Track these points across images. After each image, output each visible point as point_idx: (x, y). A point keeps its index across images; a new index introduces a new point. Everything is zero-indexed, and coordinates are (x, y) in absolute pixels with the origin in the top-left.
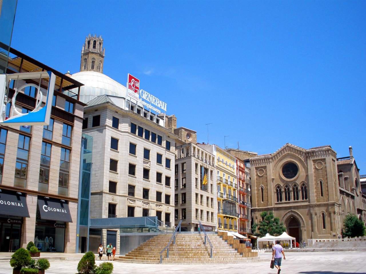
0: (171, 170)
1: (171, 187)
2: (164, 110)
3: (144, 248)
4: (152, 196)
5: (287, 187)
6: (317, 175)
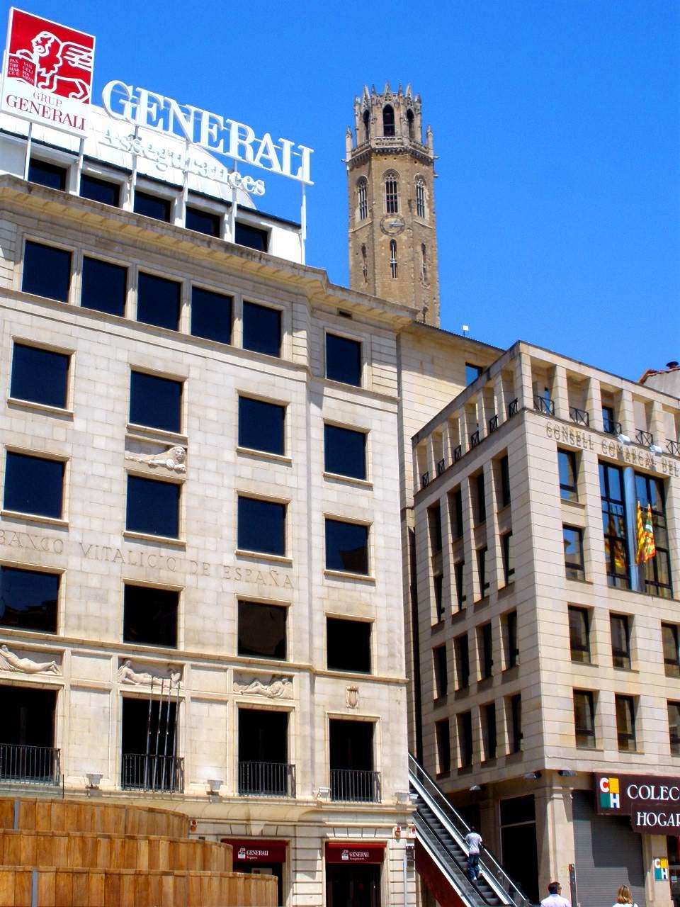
0: (370, 487)
2: (298, 177)
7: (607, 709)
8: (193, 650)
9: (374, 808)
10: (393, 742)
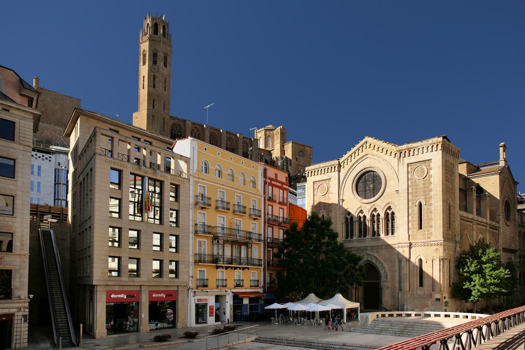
7: (35, 184)
10: (20, 277)
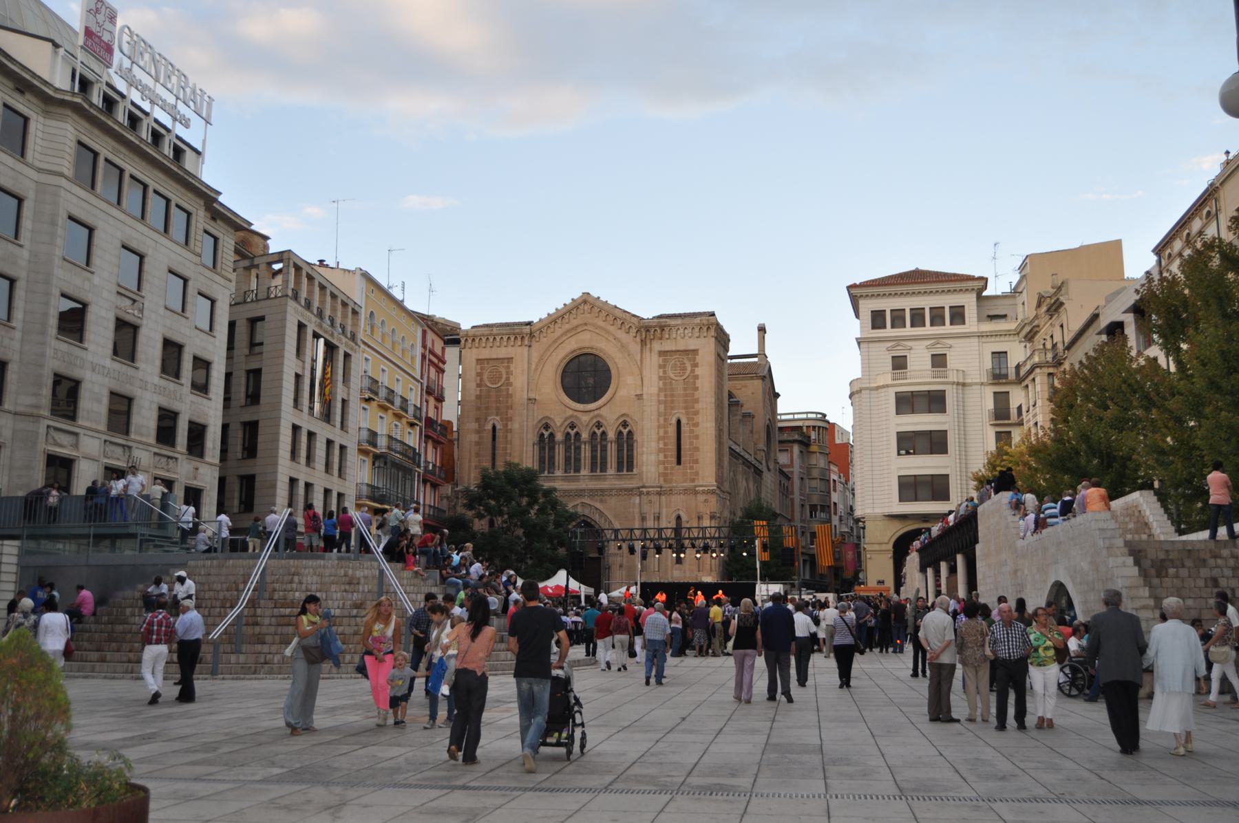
1: (211, 395)
3: (133, 615)
4: (145, 420)
5: (599, 429)
6: (669, 399)
8: (138, 438)
9: (587, 455)
